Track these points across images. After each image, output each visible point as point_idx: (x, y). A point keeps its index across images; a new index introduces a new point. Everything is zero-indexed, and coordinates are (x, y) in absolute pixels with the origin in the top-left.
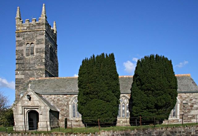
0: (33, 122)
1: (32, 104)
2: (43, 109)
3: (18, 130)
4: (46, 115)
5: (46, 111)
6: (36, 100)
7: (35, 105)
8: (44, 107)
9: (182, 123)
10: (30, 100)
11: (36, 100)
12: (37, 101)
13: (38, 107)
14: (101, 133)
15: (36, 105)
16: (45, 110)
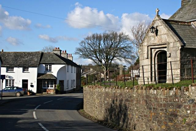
0: (159, 75)
1: (158, 41)
2: (172, 47)
3: (178, 42)
4: (176, 57)
5: (176, 51)
6: (164, 34)
7: (162, 42)
8: (174, 43)
9: (172, 82)
10: (157, 35)
11: (164, 34)
12: (165, 34)
13: (167, 43)
14: (190, 89)
15: (163, 41)
16: (174, 49)
